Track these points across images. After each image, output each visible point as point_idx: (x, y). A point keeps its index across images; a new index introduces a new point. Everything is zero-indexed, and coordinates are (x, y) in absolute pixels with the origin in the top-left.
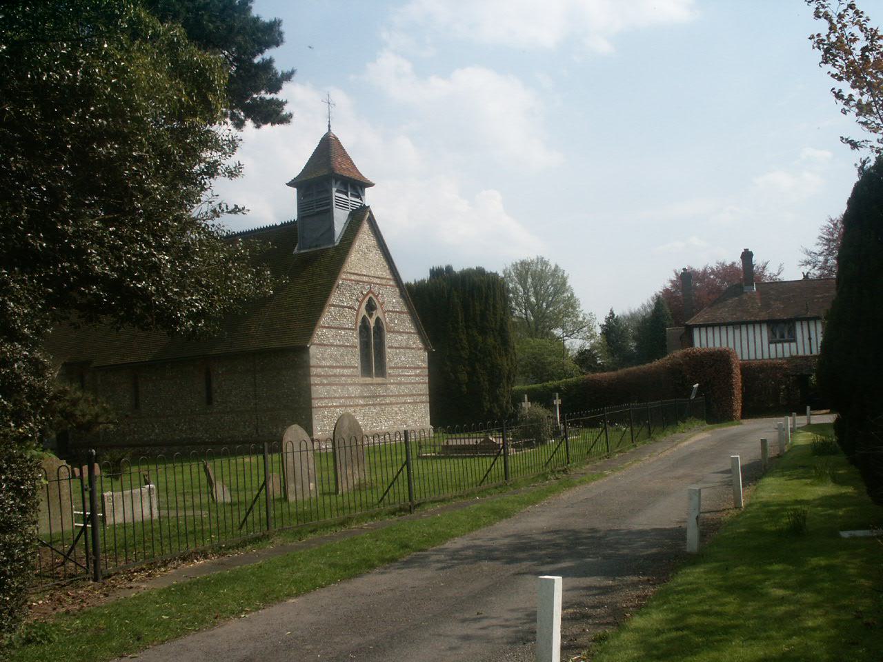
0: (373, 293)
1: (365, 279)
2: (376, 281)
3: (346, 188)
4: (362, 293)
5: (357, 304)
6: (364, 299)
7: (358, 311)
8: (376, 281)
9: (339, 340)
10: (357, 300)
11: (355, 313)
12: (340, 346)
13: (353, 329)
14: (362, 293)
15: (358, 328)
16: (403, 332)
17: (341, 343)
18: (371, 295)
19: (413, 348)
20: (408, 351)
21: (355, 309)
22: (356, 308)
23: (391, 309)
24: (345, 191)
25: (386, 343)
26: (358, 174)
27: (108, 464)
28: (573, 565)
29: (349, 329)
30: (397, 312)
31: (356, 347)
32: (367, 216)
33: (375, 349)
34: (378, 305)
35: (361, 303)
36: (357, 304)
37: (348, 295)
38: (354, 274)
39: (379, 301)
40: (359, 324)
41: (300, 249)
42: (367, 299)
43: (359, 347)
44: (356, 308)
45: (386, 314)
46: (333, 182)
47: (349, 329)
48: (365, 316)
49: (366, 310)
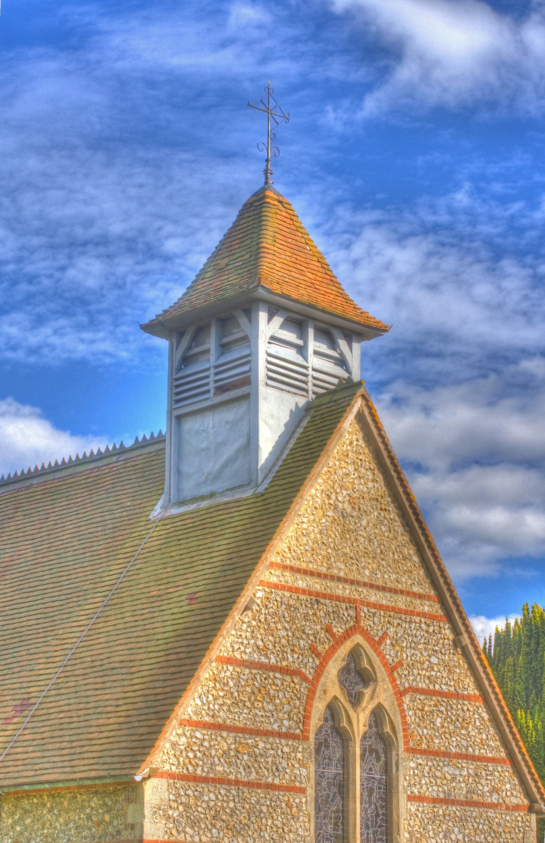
0: (365, 634)
1: (340, 590)
2: (374, 597)
3: (303, 335)
4: (328, 630)
5: (313, 662)
6: (333, 649)
7: (314, 683)
8: (374, 597)
9: (247, 767)
10: (313, 649)
11: (304, 688)
12: (249, 784)
13: (295, 737)
14: (328, 630)
15: (312, 736)
16: (459, 756)
17: (253, 776)
18: (358, 638)
19: (492, 806)
20: (476, 811)
21: (304, 678)
22: (309, 673)
23: (423, 686)
24: (300, 342)
25: (402, 783)
26: (339, 300)
27: (374, 830)
28: (214, 332)
29: (280, 735)
30: (441, 694)
31: (303, 791)
32: (355, 410)
33: (367, 800)
34: (381, 672)
35: (325, 659)
36: (313, 662)
37: (283, 633)
38: (305, 572)
39: (383, 658)
40: (315, 722)
41: (165, 508)
42: (348, 646)
43: (311, 792)
44: (309, 673)
45: (407, 699)
46: (263, 316)
47: (280, 735)
48: (335, 698)
49: (342, 683)
